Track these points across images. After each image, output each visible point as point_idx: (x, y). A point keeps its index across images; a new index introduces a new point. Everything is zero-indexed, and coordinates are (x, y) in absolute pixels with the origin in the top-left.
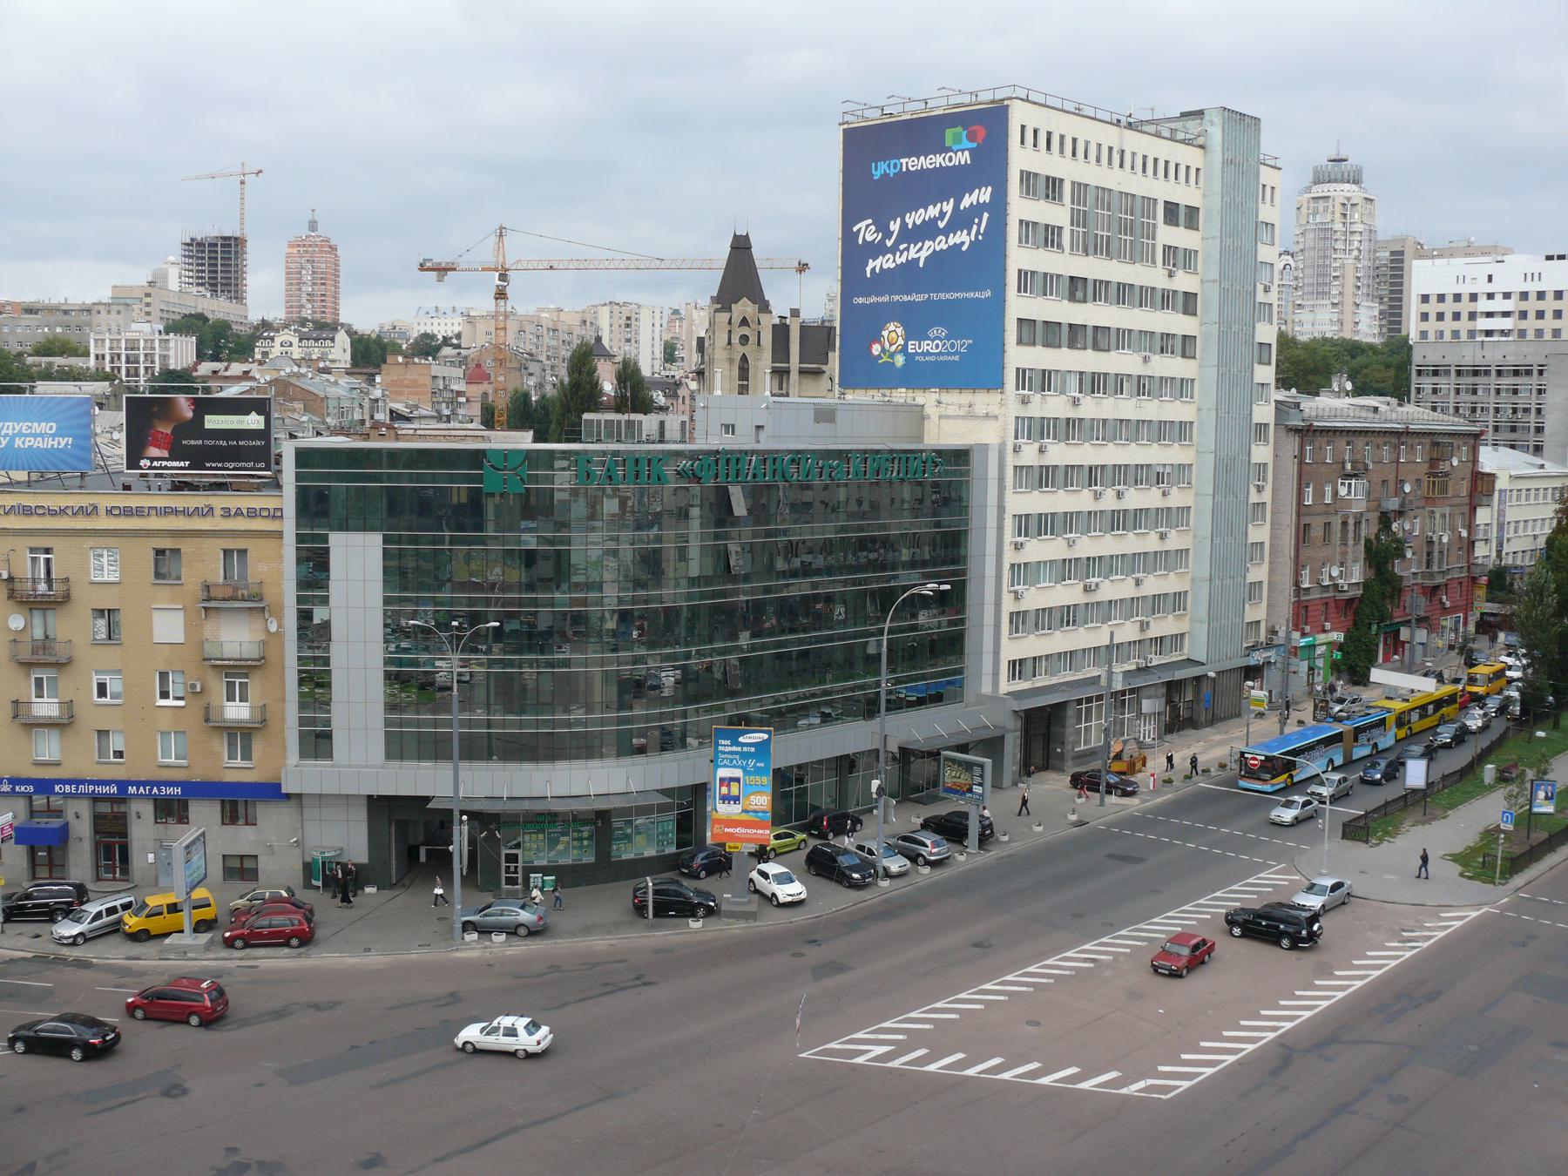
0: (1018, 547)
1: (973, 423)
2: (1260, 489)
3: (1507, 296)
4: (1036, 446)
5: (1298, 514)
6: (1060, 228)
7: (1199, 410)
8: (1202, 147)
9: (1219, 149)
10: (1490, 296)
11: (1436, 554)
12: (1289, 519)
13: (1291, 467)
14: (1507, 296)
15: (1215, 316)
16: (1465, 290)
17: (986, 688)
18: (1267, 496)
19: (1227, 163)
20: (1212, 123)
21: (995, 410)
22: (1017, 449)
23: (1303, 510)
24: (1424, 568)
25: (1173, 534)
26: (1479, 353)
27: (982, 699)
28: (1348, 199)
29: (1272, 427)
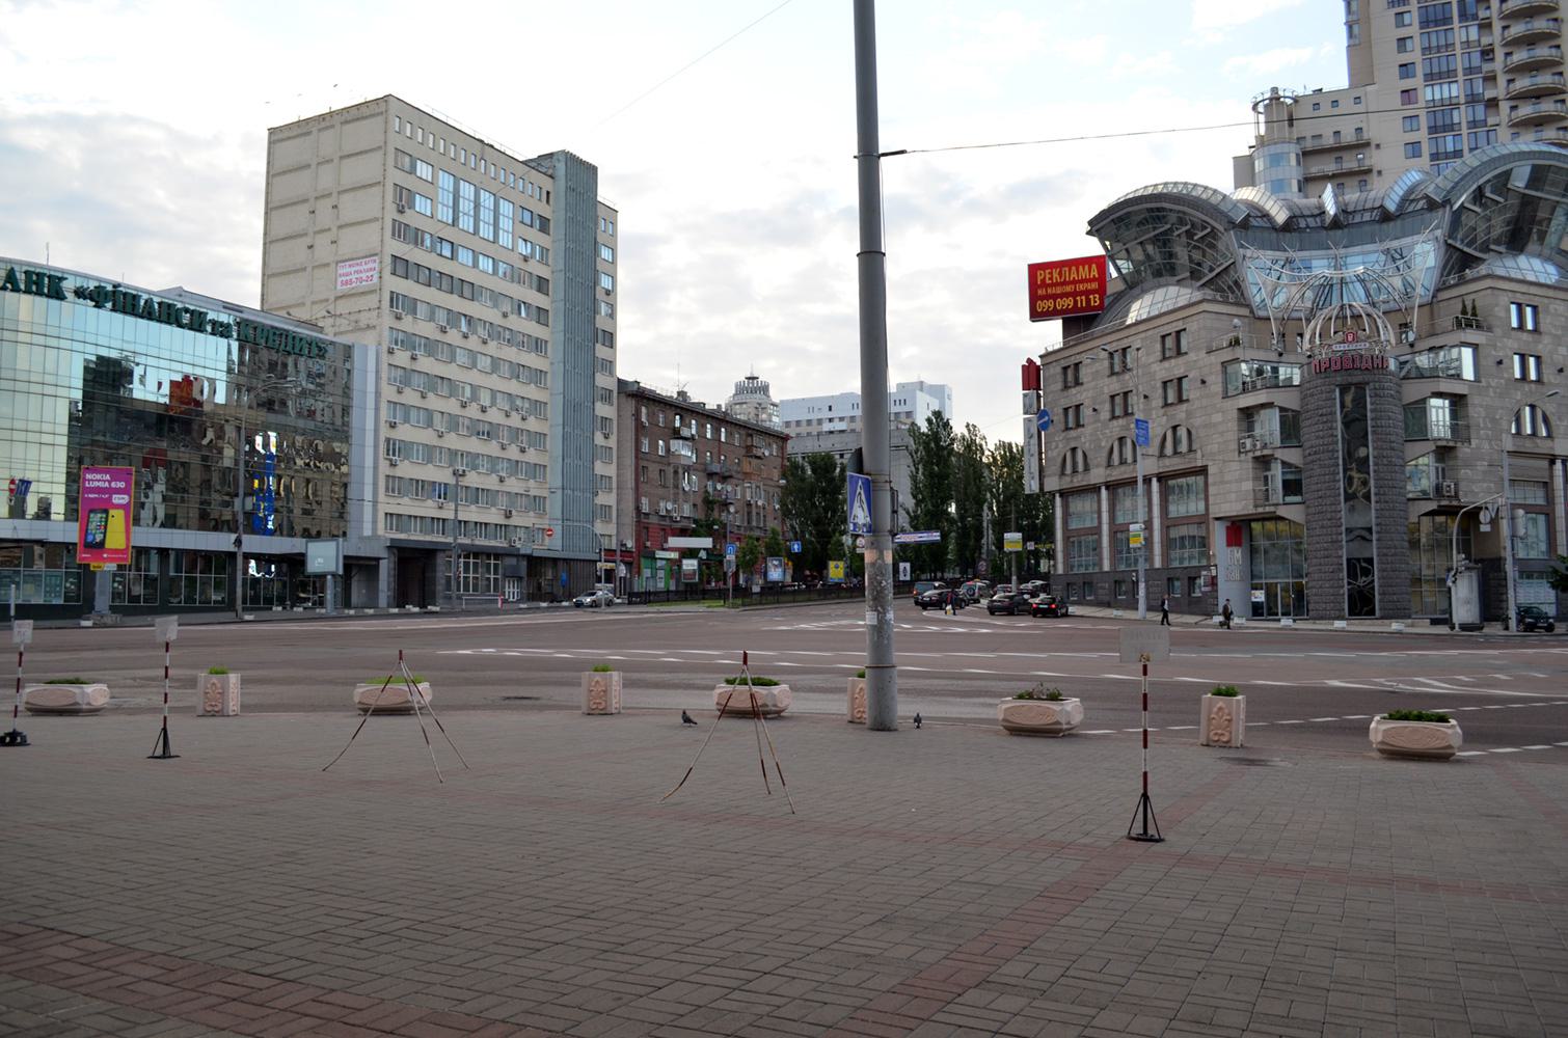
0: (393, 426)
1: (358, 334)
2: (606, 437)
3: (841, 419)
4: (409, 354)
5: (636, 457)
6: (610, 507)
7: (552, 364)
8: (551, 177)
9: (563, 178)
10: (831, 420)
11: (754, 513)
12: (629, 461)
13: (630, 423)
14: (841, 419)
15: (561, 295)
16: (814, 416)
17: (367, 532)
18: (612, 442)
19: (570, 189)
20: (558, 160)
21: (373, 322)
22: (391, 352)
23: (641, 455)
24: (746, 524)
25: (531, 451)
26: (816, 444)
27: (362, 538)
28: (760, 404)
29: (615, 394)
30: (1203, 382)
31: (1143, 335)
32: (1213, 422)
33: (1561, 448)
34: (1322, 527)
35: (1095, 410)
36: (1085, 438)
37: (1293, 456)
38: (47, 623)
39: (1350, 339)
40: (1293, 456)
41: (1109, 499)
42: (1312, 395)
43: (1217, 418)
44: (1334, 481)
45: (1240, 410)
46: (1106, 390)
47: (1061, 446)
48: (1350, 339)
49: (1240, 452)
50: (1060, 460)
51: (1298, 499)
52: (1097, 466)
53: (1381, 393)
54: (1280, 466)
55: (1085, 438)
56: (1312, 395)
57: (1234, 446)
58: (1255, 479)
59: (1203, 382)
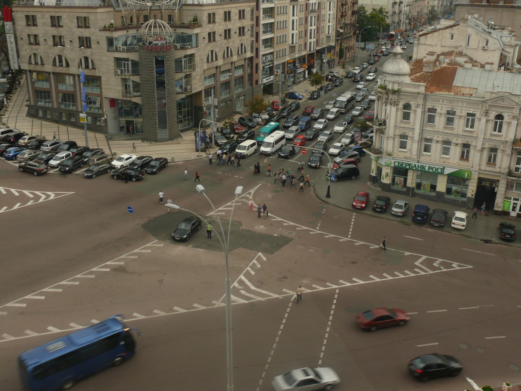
30: (98, 43)
31: (68, 13)
32: (105, 63)
33: (247, 7)
34: (149, 108)
35: (45, 40)
36: (41, 50)
37: (137, 79)
38: (90, 343)
39: (159, 39)
40: (137, 79)
41: (54, 79)
42: (145, 59)
43: (105, 58)
44: (152, 73)
45: (115, 58)
46: (50, 32)
47: (28, 50)
48: (159, 39)
49: (115, 75)
50: (28, 57)
51: (138, 94)
52: (48, 64)
53: (169, 59)
54: (132, 82)
55: (41, 50)
56: (145, 59)
57: (113, 72)
58: (122, 86)
59: (98, 43)
